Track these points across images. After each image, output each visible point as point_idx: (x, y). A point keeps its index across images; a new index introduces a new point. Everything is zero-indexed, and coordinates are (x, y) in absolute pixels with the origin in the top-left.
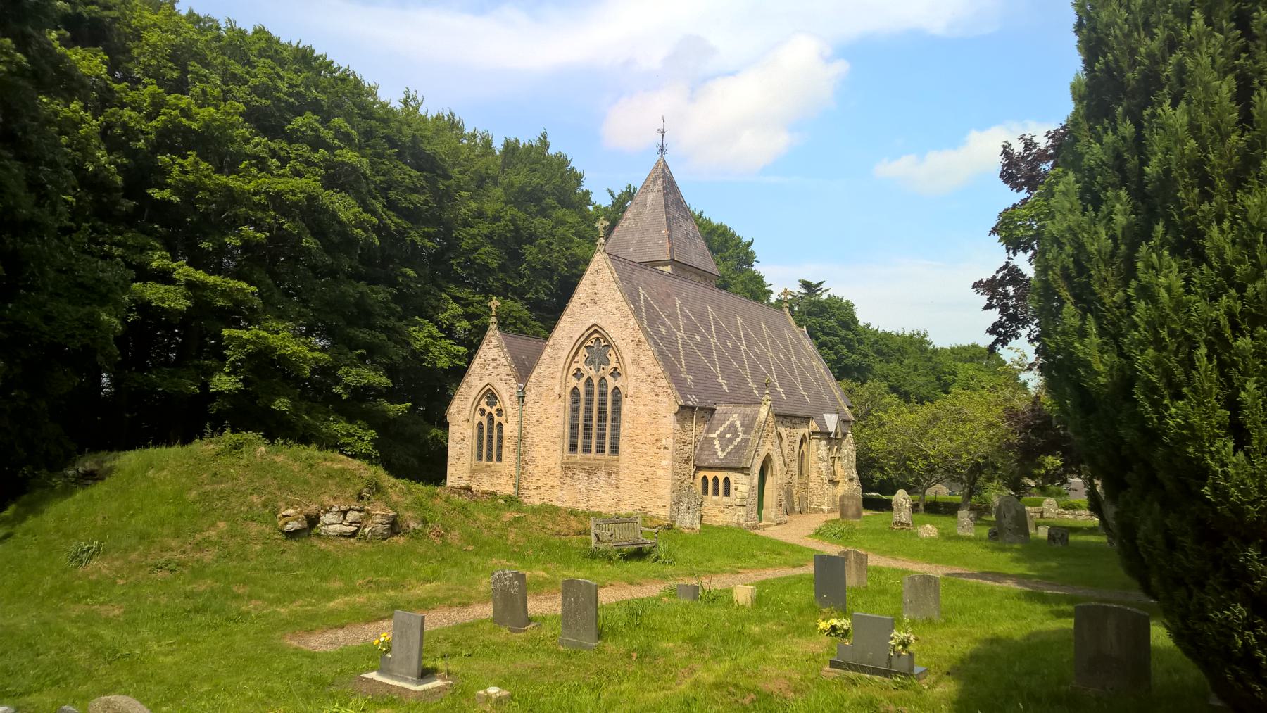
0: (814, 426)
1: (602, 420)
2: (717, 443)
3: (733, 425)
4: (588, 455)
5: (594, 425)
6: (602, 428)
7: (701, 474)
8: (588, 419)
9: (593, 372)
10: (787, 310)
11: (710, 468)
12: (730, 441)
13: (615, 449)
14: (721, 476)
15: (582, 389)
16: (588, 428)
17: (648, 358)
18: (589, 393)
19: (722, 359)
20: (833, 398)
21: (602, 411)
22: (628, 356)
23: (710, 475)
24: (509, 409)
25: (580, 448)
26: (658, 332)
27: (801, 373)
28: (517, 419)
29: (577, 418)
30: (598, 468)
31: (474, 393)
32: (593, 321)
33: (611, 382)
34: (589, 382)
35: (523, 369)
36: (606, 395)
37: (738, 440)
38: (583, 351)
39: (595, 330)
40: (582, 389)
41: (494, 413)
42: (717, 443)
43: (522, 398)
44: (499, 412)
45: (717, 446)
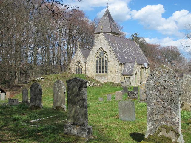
0: (142, 66)
1: (103, 66)
2: (126, 70)
3: (129, 67)
4: (101, 73)
5: (102, 67)
6: (103, 68)
7: (124, 76)
8: (100, 66)
9: (101, 57)
10: (135, 41)
11: (125, 75)
12: (129, 70)
13: (106, 72)
14: (128, 76)
15: (99, 61)
16: (100, 68)
17: (113, 54)
18: (100, 61)
19: (125, 53)
20: (145, 60)
21: (103, 65)
22: (108, 54)
23: (126, 76)
24: (83, 65)
25: (105, 72)
26: (114, 48)
27: (139, 55)
28: (85, 67)
29: (106, 68)
30: (103, 76)
31: (75, 61)
32: (100, 47)
33: (105, 59)
34: (100, 58)
35: (86, 56)
36: (104, 61)
37: (131, 69)
38: (99, 53)
39: (102, 48)
40: (99, 61)
41: (80, 66)
42: (126, 70)
43: (85, 63)
44: (81, 65)
45: (127, 71)
